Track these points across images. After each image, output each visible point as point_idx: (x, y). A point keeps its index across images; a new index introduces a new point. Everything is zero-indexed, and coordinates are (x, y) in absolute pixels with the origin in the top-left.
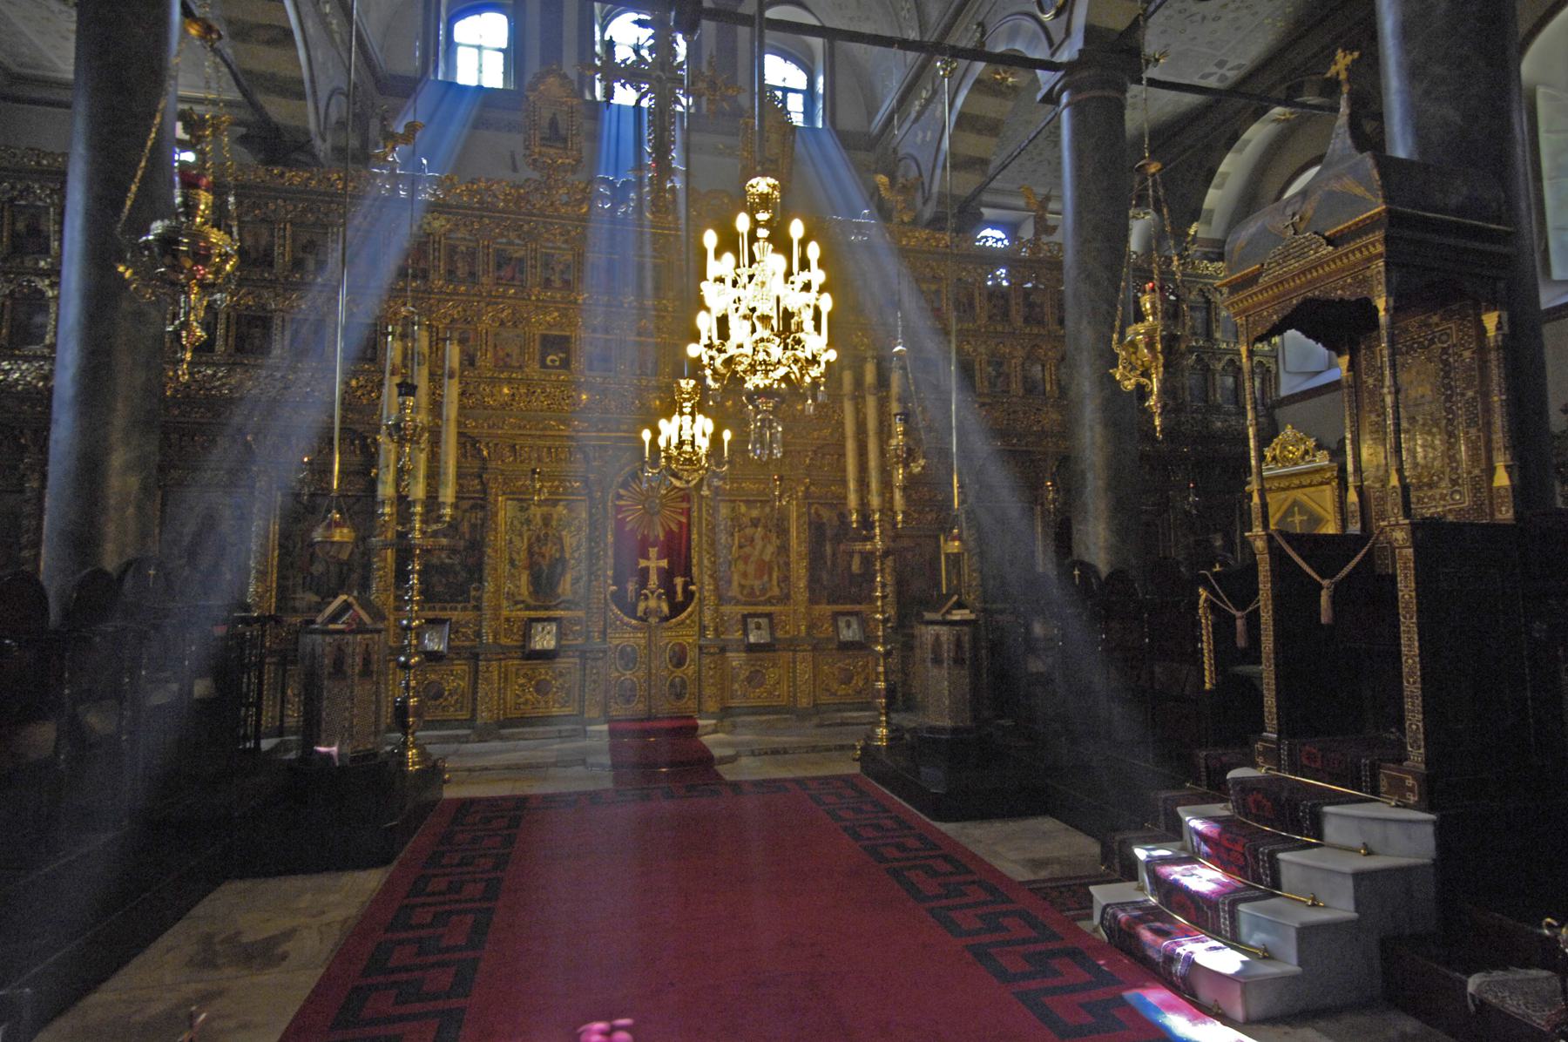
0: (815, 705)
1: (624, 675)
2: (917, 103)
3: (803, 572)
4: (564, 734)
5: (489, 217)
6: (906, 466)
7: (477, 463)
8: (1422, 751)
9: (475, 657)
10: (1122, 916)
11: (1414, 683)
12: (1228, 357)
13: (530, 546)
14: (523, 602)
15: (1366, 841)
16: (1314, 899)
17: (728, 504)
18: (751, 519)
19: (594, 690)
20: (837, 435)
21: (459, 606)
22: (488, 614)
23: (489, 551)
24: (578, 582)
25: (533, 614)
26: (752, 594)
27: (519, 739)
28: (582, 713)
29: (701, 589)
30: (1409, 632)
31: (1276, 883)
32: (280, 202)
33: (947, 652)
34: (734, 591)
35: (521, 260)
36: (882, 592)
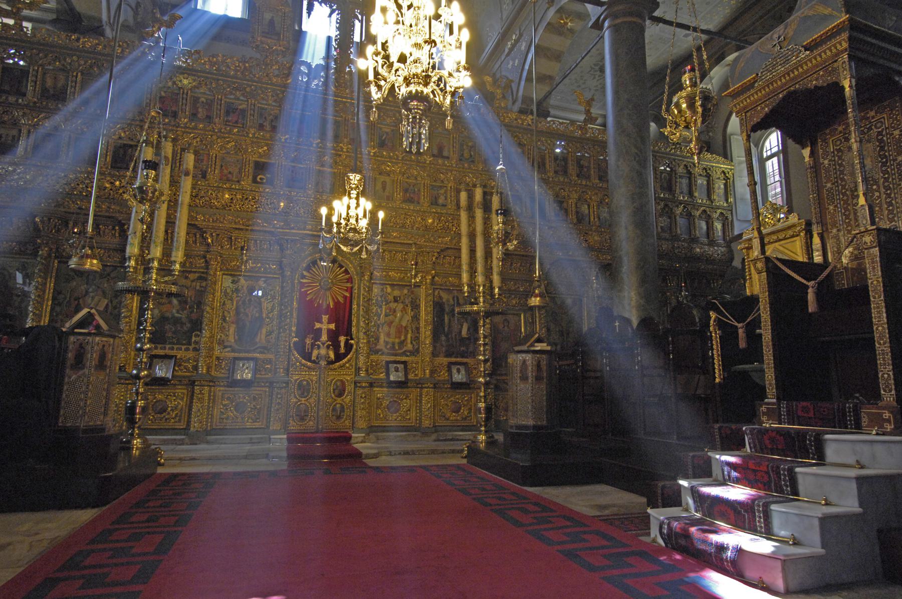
0: (435, 426)
1: (300, 401)
2: (509, 43)
3: (428, 333)
4: (253, 441)
5: (223, 80)
6: (504, 244)
7: (203, 248)
8: (893, 392)
9: (192, 383)
10: (675, 524)
11: (885, 343)
12: (702, 209)
13: (237, 309)
14: (230, 347)
15: (858, 459)
16: (826, 500)
17: (379, 286)
18: (394, 297)
19: (278, 410)
20: (454, 242)
21: (183, 347)
22: (203, 352)
23: (208, 309)
24: (270, 334)
25: (236, 355)
26: (393, 348)
27: (222, 443)
28: (268, 427)
29: (357, 343)
30: (878, 307)
31: (796, 493)
32: (75, 58)
33: (530, 373)
34: (381, 345)
35: (243, 111)
36: (484, 341)
